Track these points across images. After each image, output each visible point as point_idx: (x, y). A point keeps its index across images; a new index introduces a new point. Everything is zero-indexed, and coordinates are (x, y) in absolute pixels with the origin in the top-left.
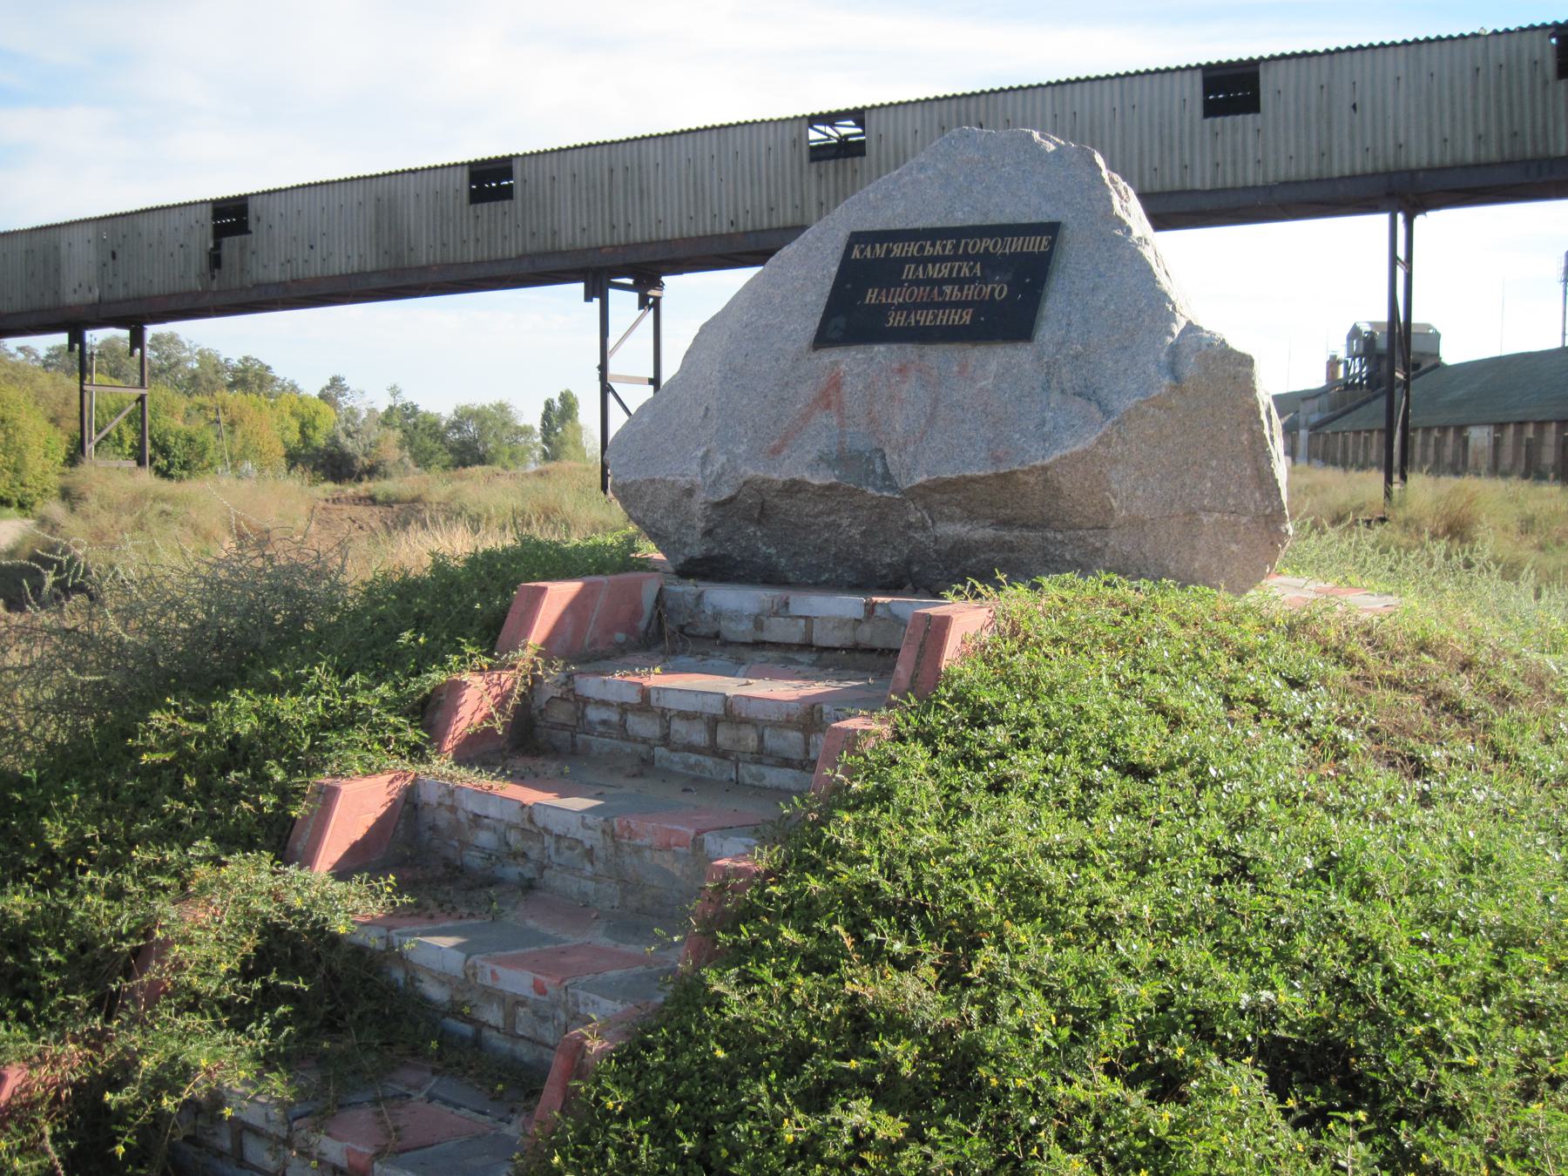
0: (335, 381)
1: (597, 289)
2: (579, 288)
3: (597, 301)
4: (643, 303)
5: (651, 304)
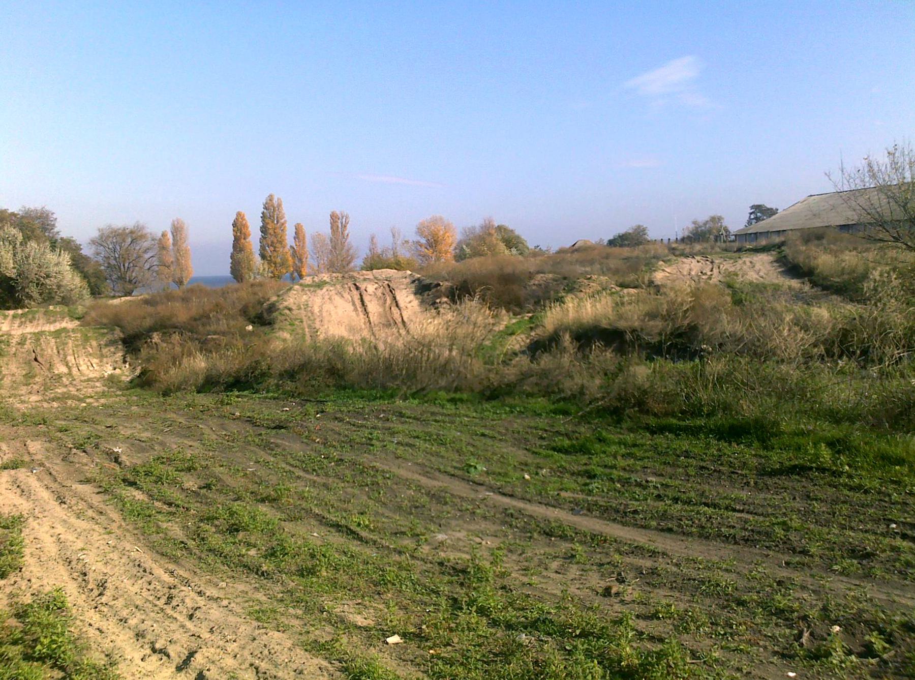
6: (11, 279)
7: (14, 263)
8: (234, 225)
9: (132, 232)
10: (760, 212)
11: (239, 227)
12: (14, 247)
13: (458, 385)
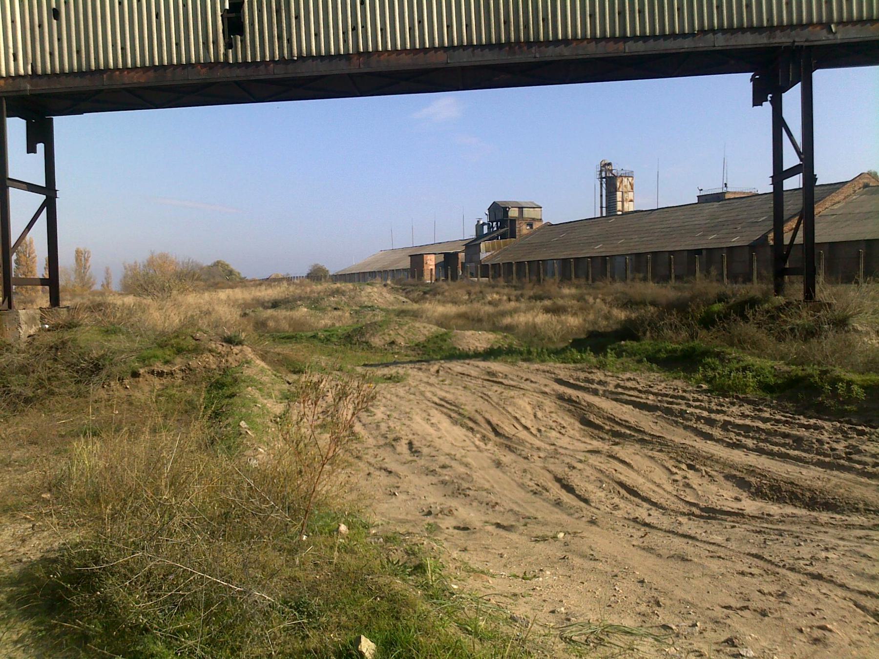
0: (77, 252)
3: (767, 107)
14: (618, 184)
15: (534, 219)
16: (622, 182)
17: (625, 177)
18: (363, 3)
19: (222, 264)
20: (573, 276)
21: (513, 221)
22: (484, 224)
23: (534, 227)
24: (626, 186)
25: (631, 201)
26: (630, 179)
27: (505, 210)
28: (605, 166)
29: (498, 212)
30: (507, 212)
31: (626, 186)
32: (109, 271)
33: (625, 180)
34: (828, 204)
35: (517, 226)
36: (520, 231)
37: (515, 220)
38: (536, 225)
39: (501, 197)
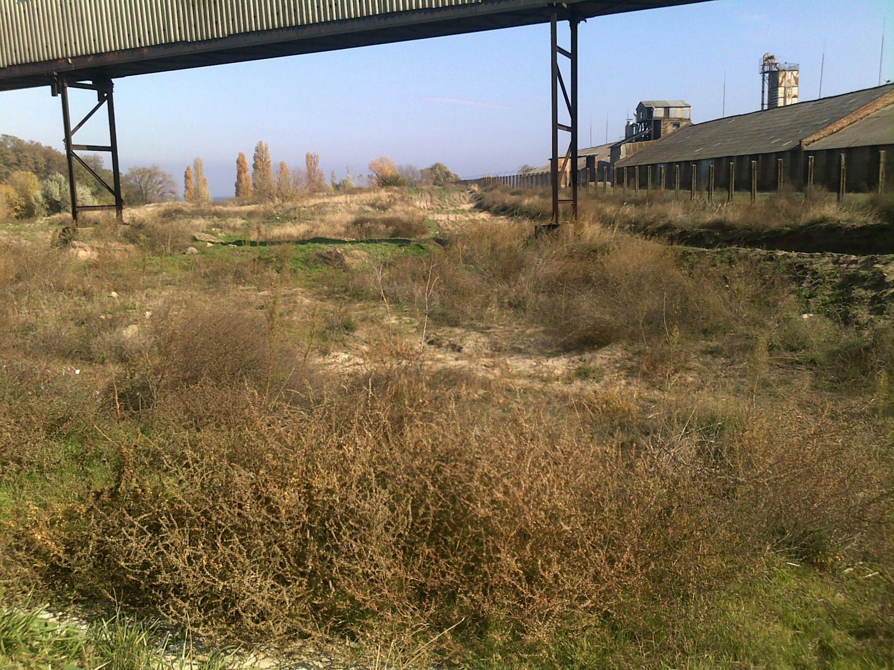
0: (307, 156)
1: (59, 90)
2: (48, 89)
3: (60, 95)
4: (101, 100)
5: (106, 95)
6: (58, 202)
7: (60, 193)
8: (238, 162)
9: (149, 171)
10: (32, 142)
11: (240, 163)
12: (60, 185)
13: (660, 189)
14: (780, 79)
15: (681, 119)
16: (784, 77)
17: (789, 71)
18: (215, 2)
19: (440, 166)
20: (649, 183)
21: (658, 122)
22: (633, 125)
23: (681, 125)
24: (789, 81)
25: (795, 97)
26: (795, 73)
27: (650, 110)
28: (769, 59)
29: (645, 111)
30: (652, 112)
31: (789, 81)
32: (334, 175)
33: (789, 74)
34: (880, 105)
35: (662, 127)
36: (665, 131)
37: (660, 121)
38: (683, 124)
39: (647, 98)
